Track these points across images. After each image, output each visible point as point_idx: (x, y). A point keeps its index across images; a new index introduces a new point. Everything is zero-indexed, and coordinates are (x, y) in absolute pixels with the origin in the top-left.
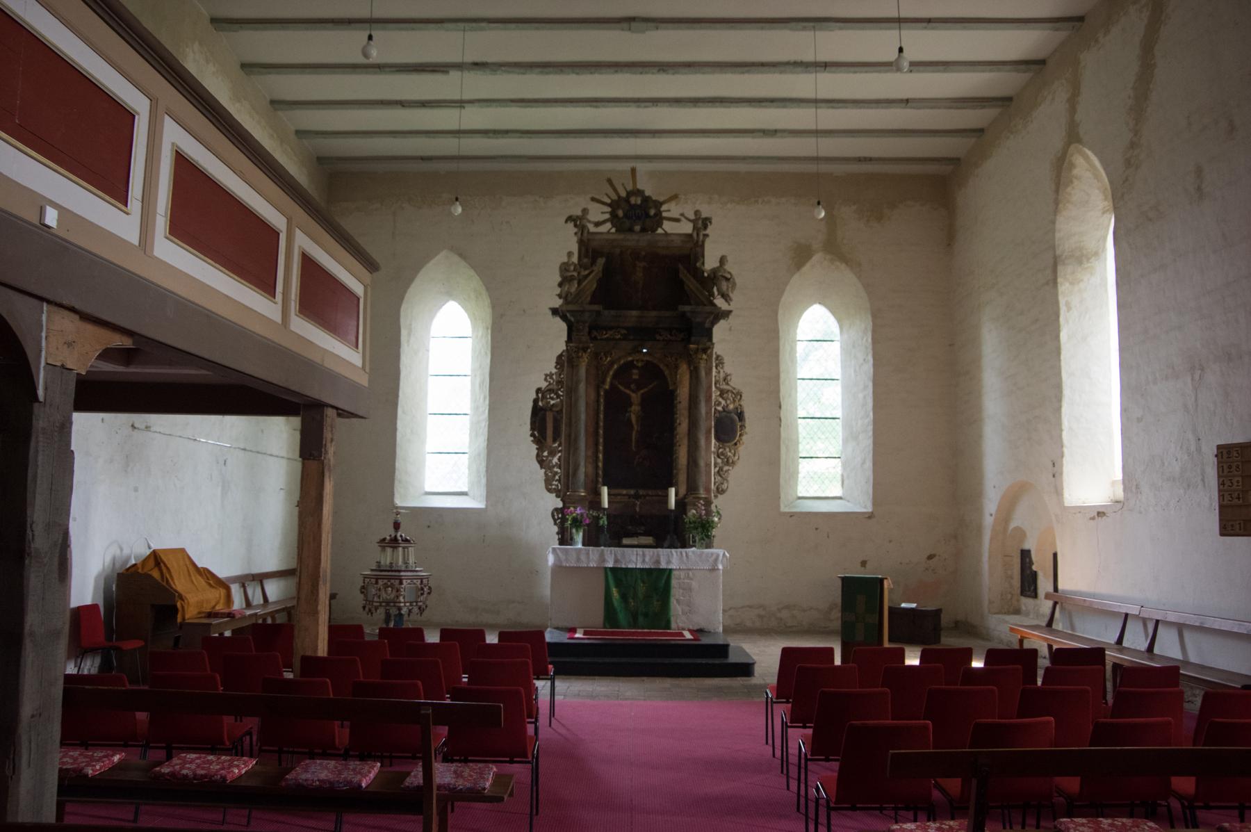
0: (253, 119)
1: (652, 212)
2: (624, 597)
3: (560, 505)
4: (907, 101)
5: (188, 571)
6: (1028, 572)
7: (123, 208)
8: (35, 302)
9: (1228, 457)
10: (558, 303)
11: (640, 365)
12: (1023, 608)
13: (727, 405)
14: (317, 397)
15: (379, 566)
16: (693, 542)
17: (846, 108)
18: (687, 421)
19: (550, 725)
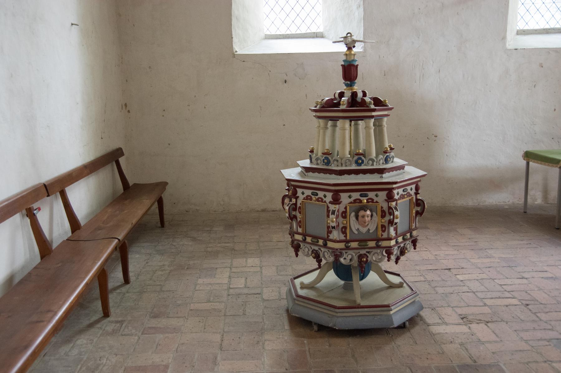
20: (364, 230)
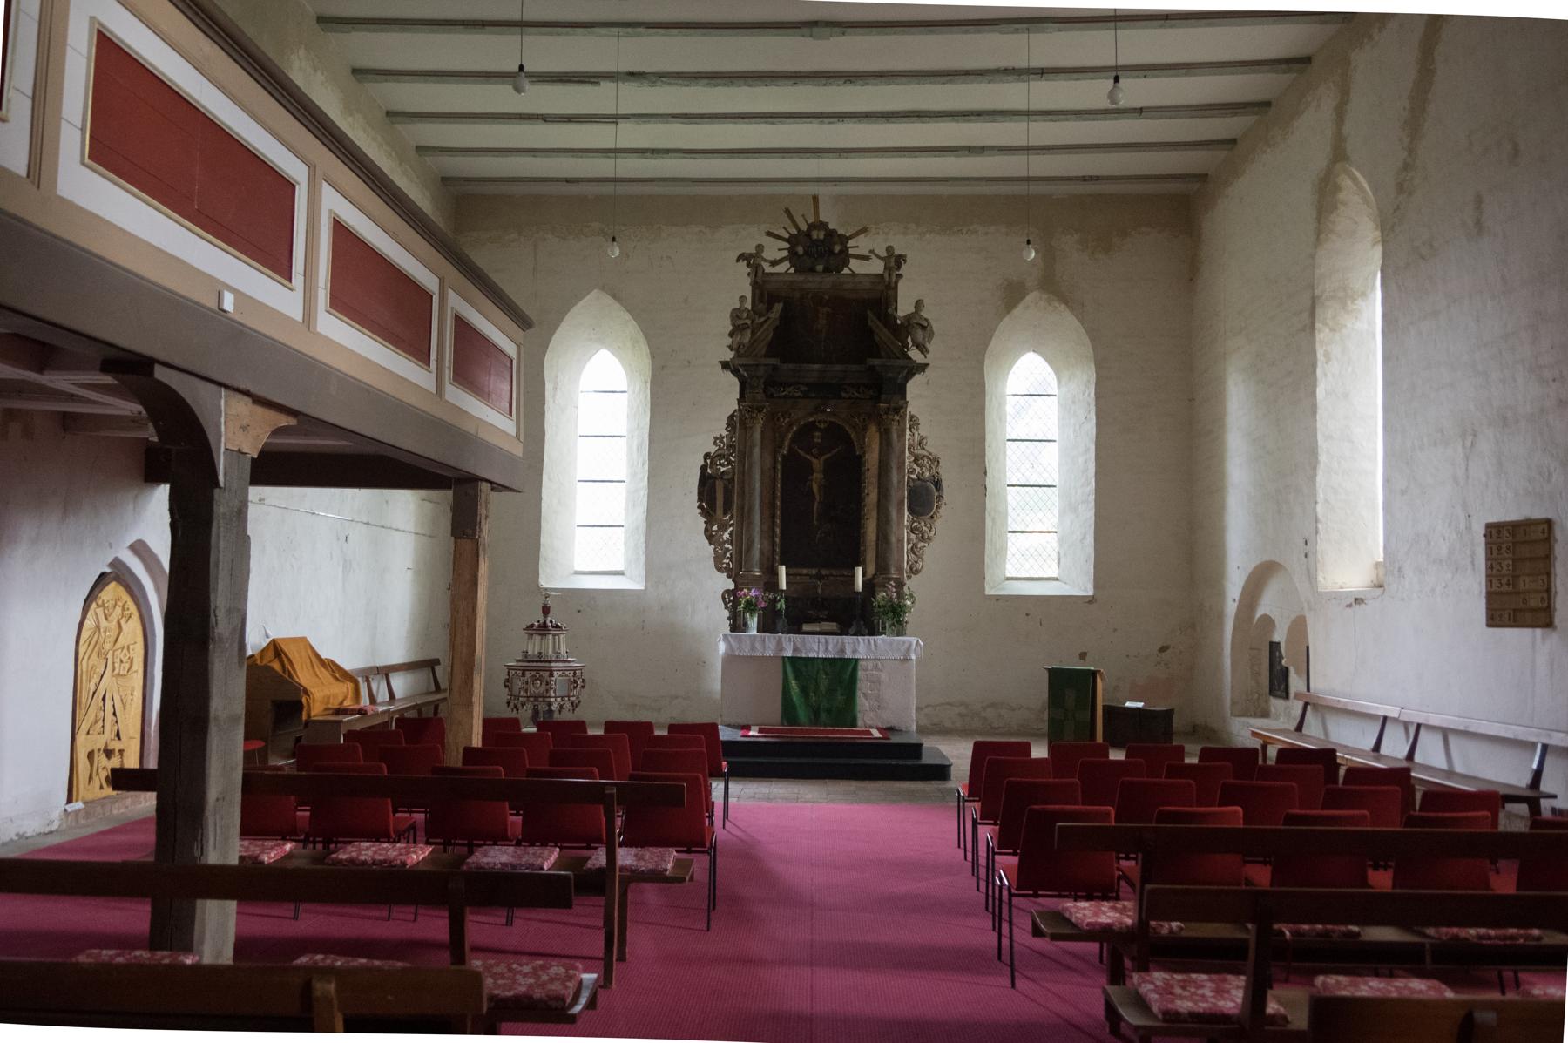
0: (368, 136)
1: (837, 249)
2: (804, 690)
3: (732, 586)
4: (1141, 110)
5: (311, 662)
6: (1278, 668)
7: (289, 285)
8: (213, 387)
9: (1498, 538)
10: (729, 355)
11: (822, 426)
12: (1273, 710)
13: (923, 472)
14: (472, 471)
15: (526, 657)
16: (882, 628)
17: (1067, 120)
18: (876, 490)
19: (724, 827)
20: (537, 692)
